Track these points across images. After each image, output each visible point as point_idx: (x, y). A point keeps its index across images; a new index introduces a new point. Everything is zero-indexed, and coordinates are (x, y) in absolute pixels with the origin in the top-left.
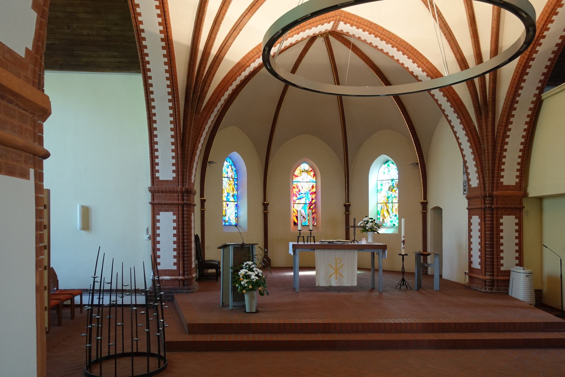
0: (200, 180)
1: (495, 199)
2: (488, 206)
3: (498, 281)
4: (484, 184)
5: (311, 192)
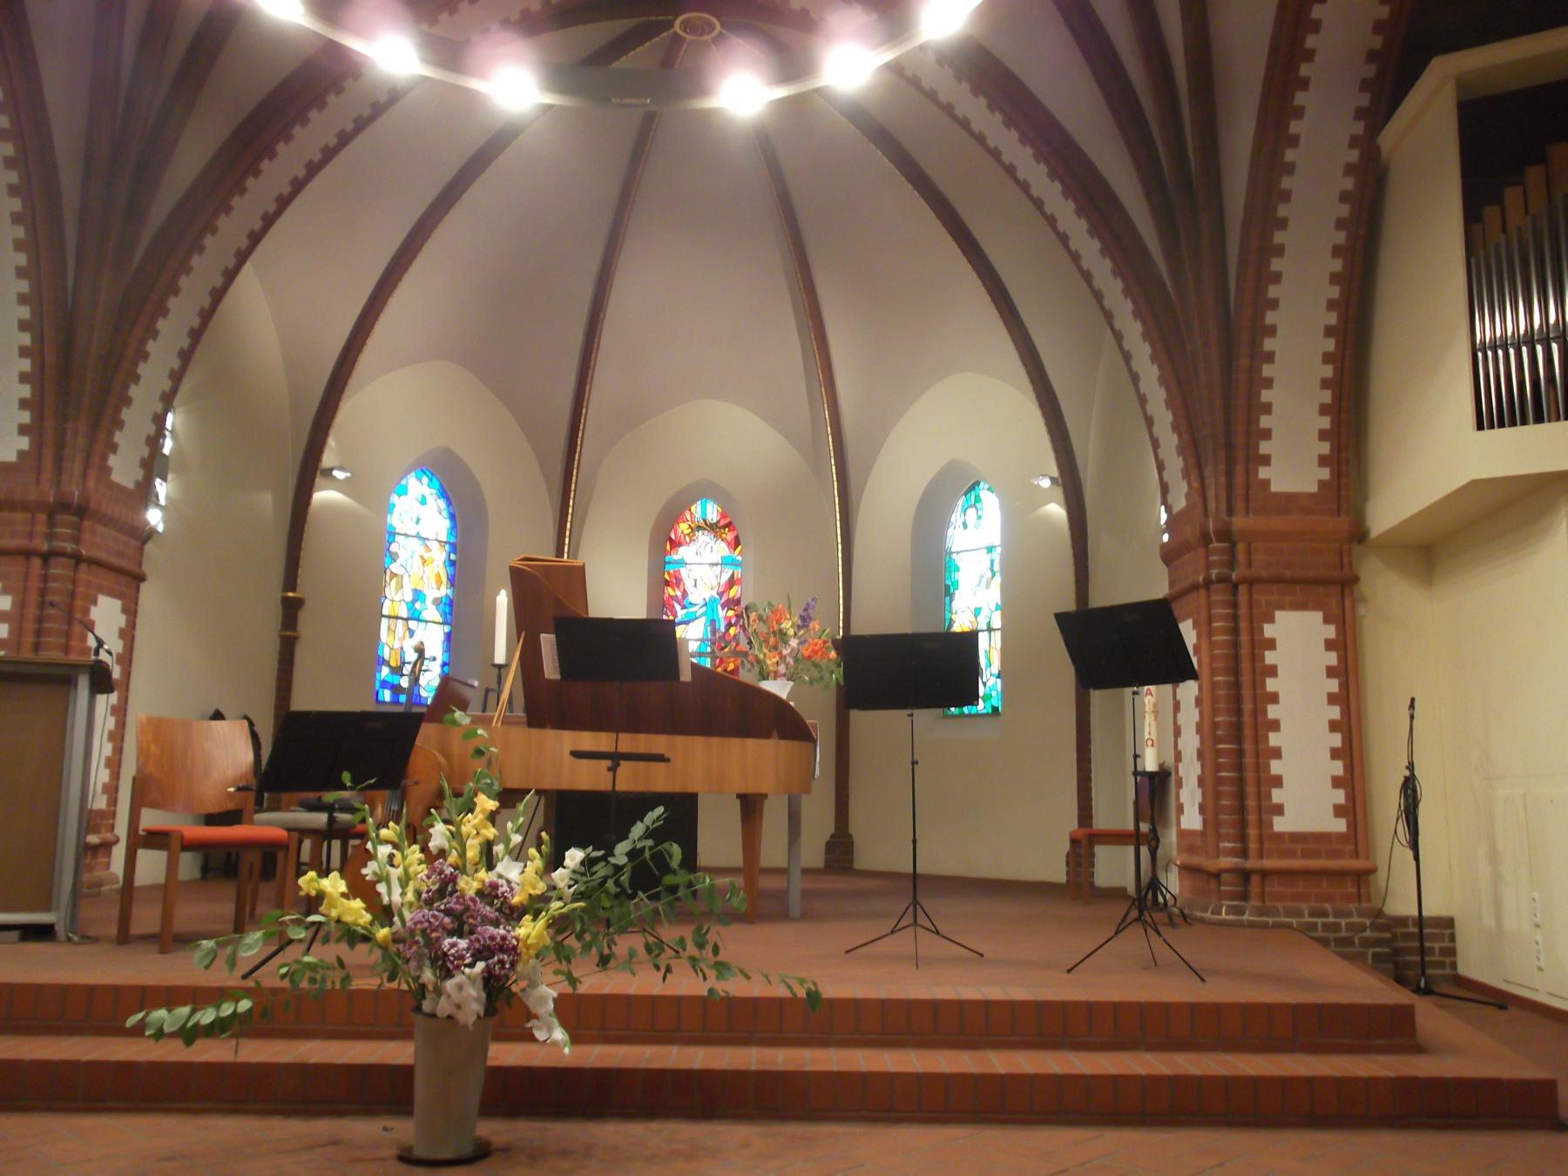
0: (287, 529)
1: (1241, 547)
2: (1214, 573)
3: (1264, 874)
4: (1203, 492)
5: (724, 599)
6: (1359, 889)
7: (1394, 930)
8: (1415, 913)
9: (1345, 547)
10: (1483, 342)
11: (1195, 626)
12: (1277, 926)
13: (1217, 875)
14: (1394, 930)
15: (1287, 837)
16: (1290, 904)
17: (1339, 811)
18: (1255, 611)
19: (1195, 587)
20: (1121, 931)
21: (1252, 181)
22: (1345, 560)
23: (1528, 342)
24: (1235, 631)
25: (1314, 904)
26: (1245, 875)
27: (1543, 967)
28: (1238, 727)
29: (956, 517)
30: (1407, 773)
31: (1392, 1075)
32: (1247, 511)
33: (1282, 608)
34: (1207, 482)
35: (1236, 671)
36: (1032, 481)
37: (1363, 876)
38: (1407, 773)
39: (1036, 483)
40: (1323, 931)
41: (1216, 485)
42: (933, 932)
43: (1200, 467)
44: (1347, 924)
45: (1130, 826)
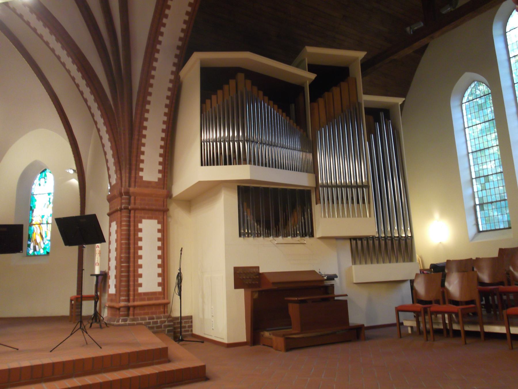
1: (132, 198)
2: (123, 206)
3: (134, 307)
4: (121, 179)
6: (164, 309)
7: (174, 322)
8: (179, 315)
9: (165, 200)
10: (204, 140)
11: (117, 224)
12: (138, 324)
13: (119, 309)
14: (174, 322)
15: (142, 294)
16: (143, 316)
17: (159, 284)
18: (136, 219)
19: (116, 211)
20: (73, 333)
21: (141, 78)
22: (165, 204)
23: (232, 141)
24: (129, 226)
25: (150, 316)
26: (128, 308)
27: (214, 329)
28: (129, 258)
29: (36, 181)
30: (179, 271)
31: (157, 372)
32: (135, 186)
33: (145, 218)
34: (123, 175)
35: (129, 239)
36: (66, 170)
37: (165, 305)
38: (179, 271)
39: (68, 171)
40: (189, 321)
41: (126, 176)
42: (72, 333)
43: (120, 170)
44: (160, 321)
45: (93, 293)
